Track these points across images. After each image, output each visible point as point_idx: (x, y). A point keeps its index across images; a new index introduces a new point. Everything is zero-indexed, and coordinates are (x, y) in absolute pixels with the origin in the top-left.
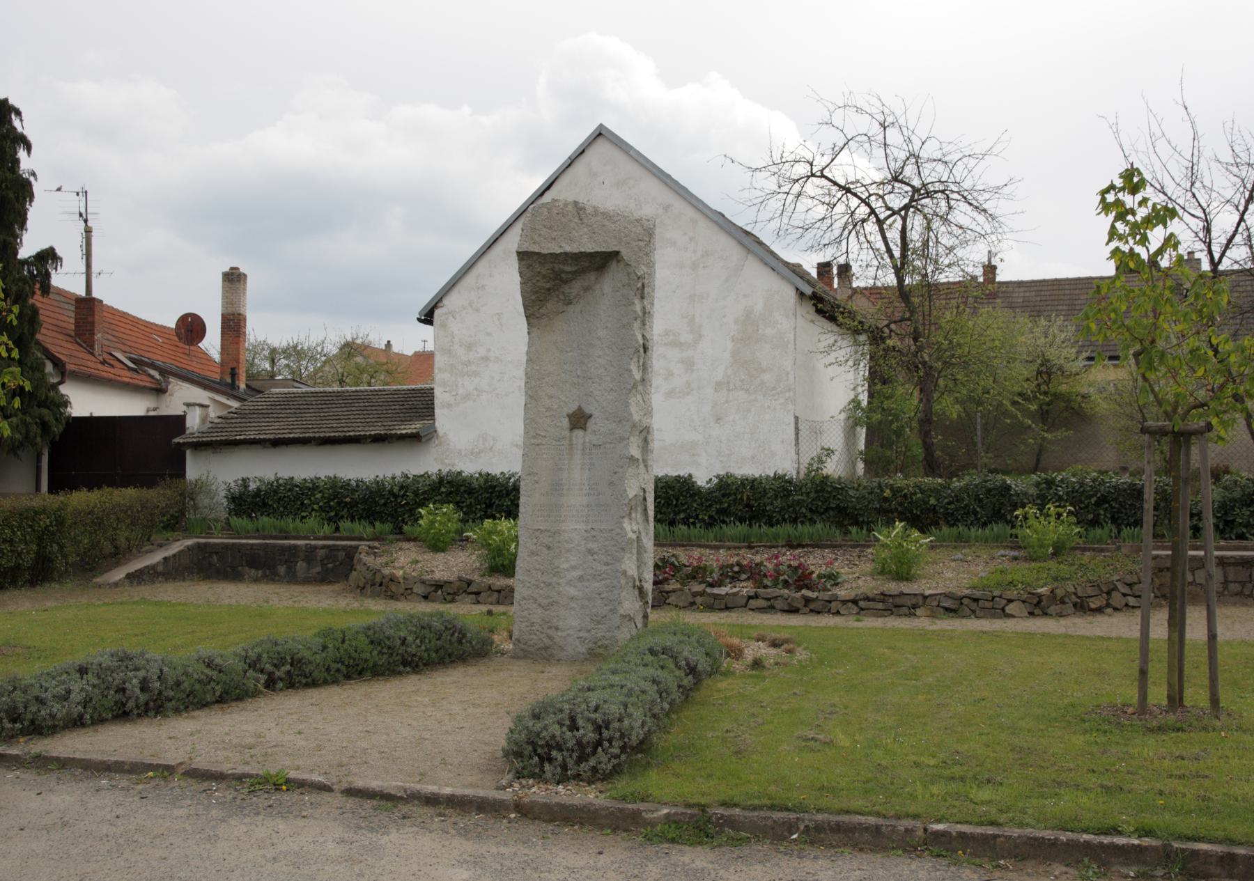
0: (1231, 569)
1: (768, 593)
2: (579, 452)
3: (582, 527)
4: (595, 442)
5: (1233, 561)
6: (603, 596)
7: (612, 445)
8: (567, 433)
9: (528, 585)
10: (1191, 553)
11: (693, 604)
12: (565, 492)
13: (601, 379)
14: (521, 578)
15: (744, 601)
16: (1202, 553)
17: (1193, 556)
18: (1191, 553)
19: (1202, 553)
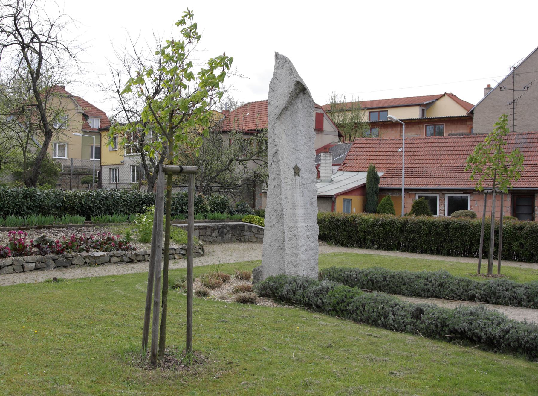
0: (201, 230)
1: (68, 255)
2: (299, 187)
3: (303, 224)
4: (304, 183)
5: (202, 227)
6: (313, 258)
7: (310, 185)
8: (293, 177)
9: (290, 256)
10: (195, 224)
11: (86, 263)
12: (296, 207)
13: (302, 151)
14: (287, 252)
15: (109, 258)
16: (186, 225)
17: (196, 226)
18: (195, 224)
19: (186, 225)
